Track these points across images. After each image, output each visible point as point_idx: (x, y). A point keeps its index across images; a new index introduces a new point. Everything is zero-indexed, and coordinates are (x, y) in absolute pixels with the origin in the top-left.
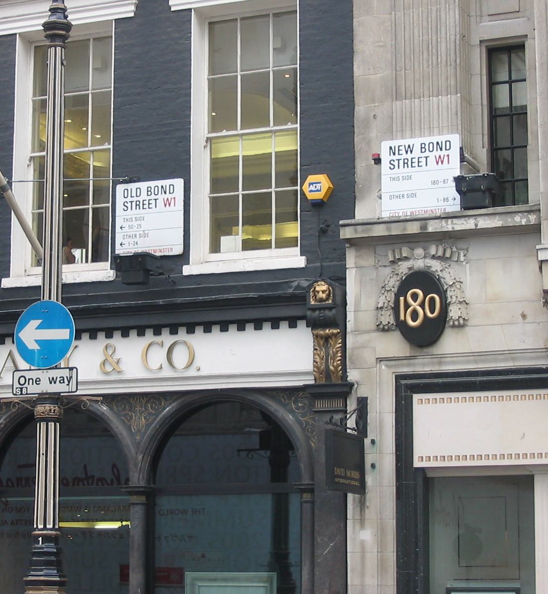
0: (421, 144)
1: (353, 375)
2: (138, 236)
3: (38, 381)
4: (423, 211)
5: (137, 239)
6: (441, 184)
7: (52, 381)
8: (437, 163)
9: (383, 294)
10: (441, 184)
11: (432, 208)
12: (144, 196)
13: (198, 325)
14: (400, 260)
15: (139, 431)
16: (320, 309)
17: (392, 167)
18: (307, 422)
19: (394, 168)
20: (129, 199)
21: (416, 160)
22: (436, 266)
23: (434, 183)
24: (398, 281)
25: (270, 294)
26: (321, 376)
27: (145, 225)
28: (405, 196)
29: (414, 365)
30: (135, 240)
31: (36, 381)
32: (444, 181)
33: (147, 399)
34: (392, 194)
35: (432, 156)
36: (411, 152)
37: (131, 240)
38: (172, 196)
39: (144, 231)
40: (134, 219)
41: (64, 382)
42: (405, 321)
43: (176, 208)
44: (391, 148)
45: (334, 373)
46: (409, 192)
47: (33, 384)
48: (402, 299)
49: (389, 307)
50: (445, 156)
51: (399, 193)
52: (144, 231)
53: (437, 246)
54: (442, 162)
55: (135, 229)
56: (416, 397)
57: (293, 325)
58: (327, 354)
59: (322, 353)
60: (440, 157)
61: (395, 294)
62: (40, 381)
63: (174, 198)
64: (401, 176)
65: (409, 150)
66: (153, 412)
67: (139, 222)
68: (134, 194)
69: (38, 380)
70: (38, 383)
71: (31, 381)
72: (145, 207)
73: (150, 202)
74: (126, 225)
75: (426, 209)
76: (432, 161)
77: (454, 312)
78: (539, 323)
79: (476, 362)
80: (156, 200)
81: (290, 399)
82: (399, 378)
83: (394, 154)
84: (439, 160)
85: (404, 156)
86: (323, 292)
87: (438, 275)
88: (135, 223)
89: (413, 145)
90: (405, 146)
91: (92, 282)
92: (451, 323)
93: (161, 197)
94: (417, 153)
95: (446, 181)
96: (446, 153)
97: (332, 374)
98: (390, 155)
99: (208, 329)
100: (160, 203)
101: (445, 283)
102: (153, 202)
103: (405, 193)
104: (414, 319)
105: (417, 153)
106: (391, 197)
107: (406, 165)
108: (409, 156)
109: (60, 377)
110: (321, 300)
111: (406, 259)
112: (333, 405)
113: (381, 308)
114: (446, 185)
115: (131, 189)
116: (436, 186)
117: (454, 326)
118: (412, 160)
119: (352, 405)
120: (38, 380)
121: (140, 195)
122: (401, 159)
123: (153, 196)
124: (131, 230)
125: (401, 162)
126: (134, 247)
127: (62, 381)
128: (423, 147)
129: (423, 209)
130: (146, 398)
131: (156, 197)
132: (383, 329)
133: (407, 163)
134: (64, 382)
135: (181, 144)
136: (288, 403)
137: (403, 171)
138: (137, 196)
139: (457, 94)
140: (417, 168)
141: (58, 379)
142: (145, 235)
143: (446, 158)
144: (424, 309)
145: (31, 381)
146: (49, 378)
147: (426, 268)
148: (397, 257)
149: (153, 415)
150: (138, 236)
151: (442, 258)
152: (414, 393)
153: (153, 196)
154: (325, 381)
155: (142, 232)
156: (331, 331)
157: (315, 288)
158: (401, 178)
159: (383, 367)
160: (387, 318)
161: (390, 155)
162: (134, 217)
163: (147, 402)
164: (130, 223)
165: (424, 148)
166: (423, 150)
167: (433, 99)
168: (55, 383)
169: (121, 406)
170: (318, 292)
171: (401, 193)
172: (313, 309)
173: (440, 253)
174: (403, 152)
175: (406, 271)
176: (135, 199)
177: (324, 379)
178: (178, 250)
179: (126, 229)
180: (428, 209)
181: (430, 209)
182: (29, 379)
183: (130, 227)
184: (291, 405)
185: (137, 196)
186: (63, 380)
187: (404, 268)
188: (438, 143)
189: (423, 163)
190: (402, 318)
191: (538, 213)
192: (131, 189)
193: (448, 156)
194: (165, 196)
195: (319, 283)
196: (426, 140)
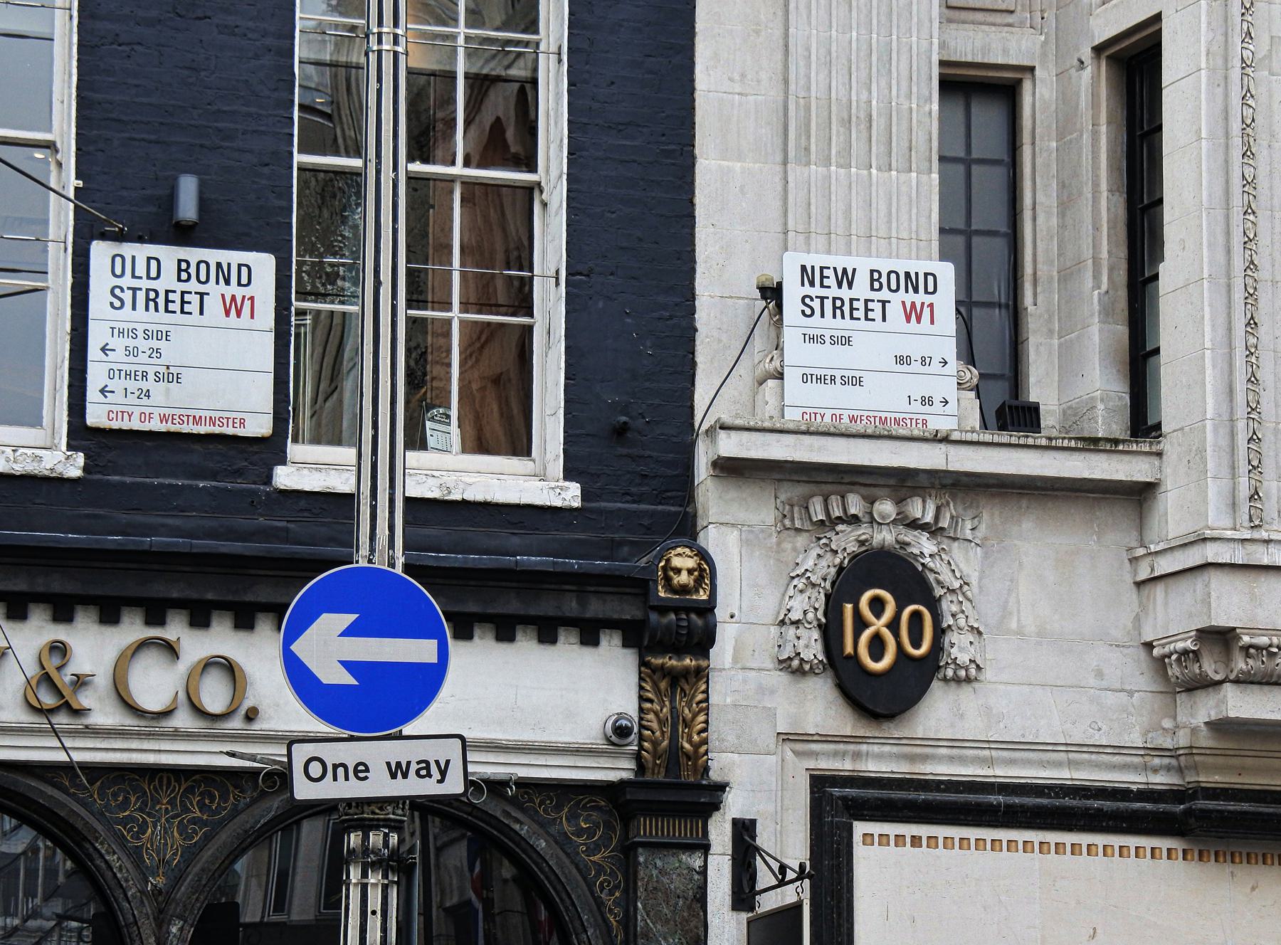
0: (872, 272)
1: (721, 764)
2: (151, 377)
3: (361, 771)
4: (877, 419)
5: (149, 384)
6: (916, 366)
7: (361, 770)
8: (227, 313)
9: (801, 591)
10: (916, 366)
11: (897, 416)
12: (168, 280)
13: (216, 609)
14: (840, 520)
15: (162, 861)
16: (677, 610)
17: (117, 304)
18: (600, 865)
19: (121, 307)
20: (127, 281)
21: (860, 305)
22: (924, 545)
23: (901, 360)
24: (835, 566)
25: (536, 563)
26: (658, 762)
27: (171, 353)
28: (838, 380)
29: (857, 756)
30: (144, 385)
31: (356, 772)
32: (923, 359)
33: (189, 783)
34: (808, 371)
35: (897, 300)
36: (850, 286)
37: (132, 385)
38: (247, 291)
39: (168, 367)
40: (140, 334)
41: (429, 775)
42: (855, 657)
43: (256, 323)
44: (804, 268)
45: (689, 758)
46: (847, 373)
47: (347, 779)
48: (849, 607)
49: (815, 623)
50: (926, 306)
51: (823, 372)
52: (168, 367)
53: (843, 497)
54: (239, 314)
55: (143, 358)
56: (860, 828)
57: (589, 638)
58: (675, 715)
59: (665, 710)
60: (913, 304)
61: (828, 596)
62: (367, 770)
63: (252, 299)
64: (140, 328)
65: (845, 278)
66: (205, 817)
67: (154, 343)
68: (141, 270)
69: (361, 768)
70: (360, 775)
71: (341, 771)
72: (856, 314)
73: (870, 305)
74: (118, 343)
75: (883, 415)
76: (895, 310)
77: (960, 648)
78: (1131, 693)
79: (1071, 764)
80: (202, 295)
81: (559, 808)
82: (820, 783)
83: (812, 284)
84: (912, 313)
85: (834, 292)
86: (690, 572)
87: (923, 564)
88: (143, 344)
89: (854, 270)
90: (835, 269)
91: (22, 476)
92: (950, 673)
93: (215, 290)
94: (861, 288)
95: (928, 360)
96: (928, 299)
97: (683, 760)
98: (803, 284)
99: (505, 634)
100: (214, 305)
101: (939, 582)
102: (195, 299)
103: (838, 374)
104: (877, 654)
105: (861, 288)
106: (805, 378)
107: (838, 312)
108: (845, 293)
109: (418, 763)
110: (684, 589)
111: (854, 520)
112: (686, 834)
113: (796, 623)
114: (926, 369)
115: (134, 257)
116: (905, 368)
117: (945, 679)
118: (851, 304)
119: (720, 833)
120: (361, 768)
121: (249, 283)
122: (828, 298)
123: (193, 285)
124: (131, 359)
125: (828, 304)
126: (138, 402)
127: (423, 772)
128: (875, 277)
129: (878, 414)
130: (186, 781)
131: (202, 288)
132: (795, 668)
133: (840, 308)
134: (429, 775)
135: (266, 170)
136: (555, 819)
137: (829, 324)
138: (149, 277)
139: (931, 173)
140: (179, 317)
141: (414, 767)
142: (170, 377)
143: (927, 311)
144: (897, 635)
145: (341, 771)
146: (388, 764)
147: (897, 546)
148: (837, 512)
149: (205, 824)
150: (151, 377)
151: (934, 530)
152: (856, 820)
153: (193, 285)
154: (666, 776)
155: (163, 370)
156: (694, 663)
157: (668, 561)
158: (827, 339)
159: (790, 753)
160: (811, 647)
161: (803, 284)
162: (140, 328)
163: (190, 790)
164: (131, 343)
165: (877, 280)
166: (876, 285)
167: (434, 186)
168: (405, 776)
169: (115, 795)
170: (678, 571)
171: (830, 372)
172: (663, 609)
173: (929, 518)
174: (831, 281)
175: (853, 548)
176: (145, 284)
177: (662, 770)
178: (261, 426)
179: (119, 355)
180: (888, 415)
181: (893, 416)
182: (335, 767)
183: (131, 352)
184: (561, 822)
185: (149, 277)
186: (428, 768)
187: (847, 541)
188: (907, 275)
189: (194, 307)
190: (849, 649)
191: (1156, 462)
192: (134, 257)
193: (931, 305)
194: (910, 297)
195: (679, 550)
196: (884, 266)
